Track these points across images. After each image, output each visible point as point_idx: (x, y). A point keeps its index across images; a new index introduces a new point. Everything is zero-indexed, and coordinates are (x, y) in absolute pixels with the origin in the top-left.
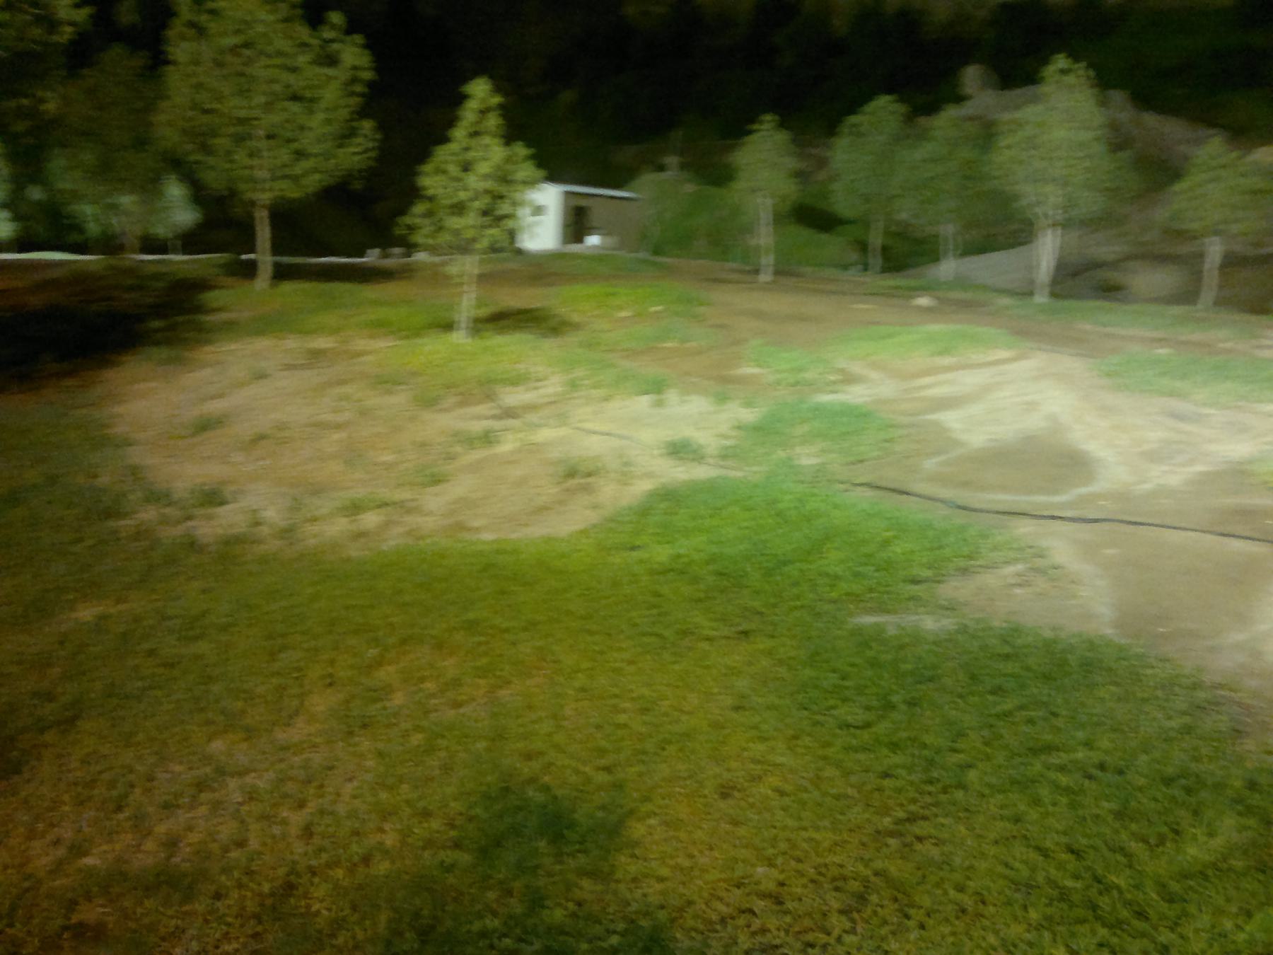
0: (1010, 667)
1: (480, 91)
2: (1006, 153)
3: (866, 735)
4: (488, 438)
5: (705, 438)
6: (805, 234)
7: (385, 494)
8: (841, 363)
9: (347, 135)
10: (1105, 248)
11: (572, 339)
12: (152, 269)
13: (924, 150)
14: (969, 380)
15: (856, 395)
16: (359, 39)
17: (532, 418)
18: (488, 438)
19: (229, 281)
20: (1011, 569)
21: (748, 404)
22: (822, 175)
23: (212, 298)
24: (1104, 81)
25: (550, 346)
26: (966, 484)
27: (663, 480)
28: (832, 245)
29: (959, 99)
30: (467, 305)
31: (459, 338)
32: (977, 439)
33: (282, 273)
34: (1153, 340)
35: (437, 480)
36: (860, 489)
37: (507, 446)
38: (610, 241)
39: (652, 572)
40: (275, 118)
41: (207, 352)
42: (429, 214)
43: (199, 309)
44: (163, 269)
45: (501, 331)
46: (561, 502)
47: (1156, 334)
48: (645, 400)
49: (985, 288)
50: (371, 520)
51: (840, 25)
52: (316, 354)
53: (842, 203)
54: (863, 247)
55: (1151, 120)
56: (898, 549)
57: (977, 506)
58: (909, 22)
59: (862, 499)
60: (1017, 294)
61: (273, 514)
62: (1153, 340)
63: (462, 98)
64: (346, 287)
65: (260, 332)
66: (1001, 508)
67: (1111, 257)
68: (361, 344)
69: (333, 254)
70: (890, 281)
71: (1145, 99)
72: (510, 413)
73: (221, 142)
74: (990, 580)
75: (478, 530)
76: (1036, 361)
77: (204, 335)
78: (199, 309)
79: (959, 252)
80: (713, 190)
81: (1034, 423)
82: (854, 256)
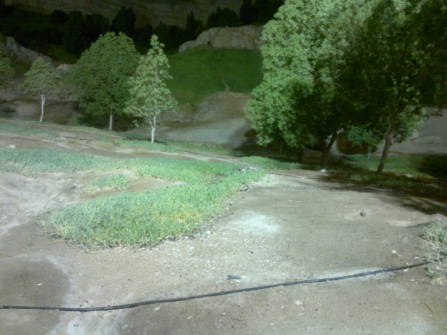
47: (15, 135)
55: (23, 49)
67: (10, 99)
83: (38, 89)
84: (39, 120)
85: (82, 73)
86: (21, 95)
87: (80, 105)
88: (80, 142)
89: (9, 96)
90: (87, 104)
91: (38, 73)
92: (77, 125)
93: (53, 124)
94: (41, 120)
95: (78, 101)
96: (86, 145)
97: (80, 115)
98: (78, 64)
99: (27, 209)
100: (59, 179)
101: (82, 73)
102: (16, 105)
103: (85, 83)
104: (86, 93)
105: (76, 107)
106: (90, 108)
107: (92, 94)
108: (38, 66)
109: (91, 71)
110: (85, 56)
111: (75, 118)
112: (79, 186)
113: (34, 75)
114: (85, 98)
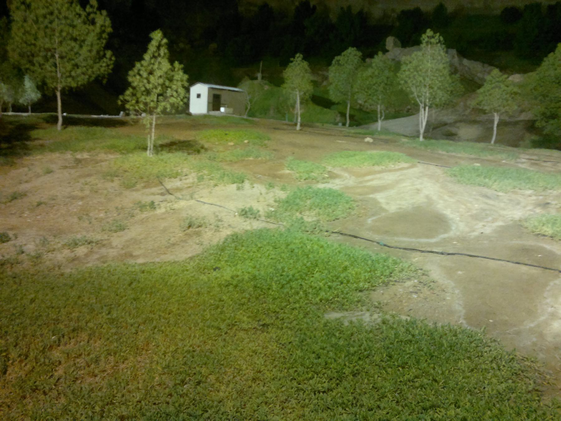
0: (410, 349)
1: (157, 36)
2: (404, 74)
3: (328, 398)
4: (152, 205)
5: (260, 207)
6: (318, 108)
7: (91, 236)
8: (329, 168)
9: (100, 57)
10: (448, 117)
11: (204, 156)
12: (12, 119)
13: (370, 71)
14: (389, 178)
15: (335, 185)
16: (104, 12)
17: (178, 195)
18: (152, 205)
19: (45, 125)
20: (408, 283)
21: (283, 189)
22: (325, 83)
23: (34, 134)
24: (449, 44)
25: (193, 159)
26: (386, 232)
27: (236, 230)
28: (330, 114)
29: (385, 51)
30: (151, 139)
31: (149, 154)
32: (393, 208)
33: (68, 122)
34: (472, 159)
35: (122, 228)
36: (336, 235)
37: (159, 211)
38: (231, 110)
39: (220, 285)
40: (64, 49)
41: (27, 160)
42: (134, 95)
43: (28, 138)
44: (16, 119)
45: (170, 151)
46: (185, 241)
47: (473, 156)
48: (234, 186)
49: (399, 135)
50: (81, 251)
51: (333, 18)
52: (78, 161)
53: (333, 96)
54: (343, 115)
55: (466, 62)
56: (352, 271)
57: (392, 245)
58: (363, 17)
59: (334, 241)
60: (411, 137)
61: (30, 248)
62: (472, 159)
63: (150, 40)
64: (98, 129)
65: (52, 151)
66: (403, 246)
67: (452, 121)
68: (102, 156)
69: (105, 114)
70: (353, 130)
71: (463, 53)
72: (168, 192)
73: (39, 59)
74: (399, 289)
75: (138, 257)
76: (419, 169)
77: (27, 151)
78: (28, 138)
79: (383, 118)
80: (276, 89)
81: (420, 199)
82: (338, 119)
83: (492, 107)
84: (490, 142)
85: (542, 84)
86: (464, 115)
87: (538, 124)
88: (545, 164)
89: (450, 117)
90: (547, 122)
91: (493, 88)
92: (531, 148)
93: (508, 147)
94: (492, 142)
95: (535, 119)
96: (552, 168)
97: (535, 137)
98: (537, 72)
99: (507, 215)
100: (530, 196)
101: (542, 84)
102: (458, 128)
103: (545, 96)
104: (546, 108)
105: (531, 127)
106: (549, 127)
107: (555, 109)
108: (494, 81)
109: (554, 80)
110: (549, 61)
111: (527, 142)
112: (554, 203)
113: (488, 91)
114: (544, 114)
